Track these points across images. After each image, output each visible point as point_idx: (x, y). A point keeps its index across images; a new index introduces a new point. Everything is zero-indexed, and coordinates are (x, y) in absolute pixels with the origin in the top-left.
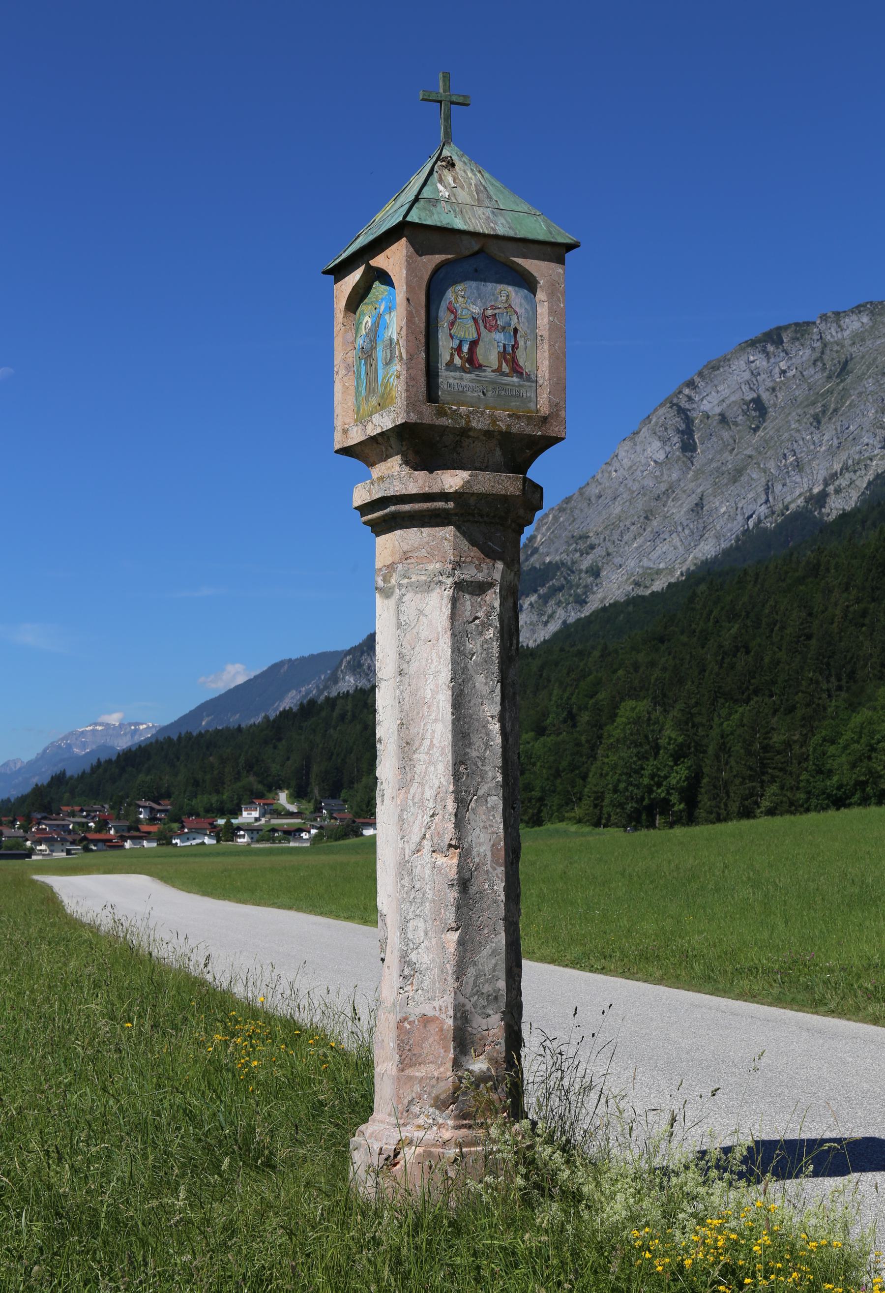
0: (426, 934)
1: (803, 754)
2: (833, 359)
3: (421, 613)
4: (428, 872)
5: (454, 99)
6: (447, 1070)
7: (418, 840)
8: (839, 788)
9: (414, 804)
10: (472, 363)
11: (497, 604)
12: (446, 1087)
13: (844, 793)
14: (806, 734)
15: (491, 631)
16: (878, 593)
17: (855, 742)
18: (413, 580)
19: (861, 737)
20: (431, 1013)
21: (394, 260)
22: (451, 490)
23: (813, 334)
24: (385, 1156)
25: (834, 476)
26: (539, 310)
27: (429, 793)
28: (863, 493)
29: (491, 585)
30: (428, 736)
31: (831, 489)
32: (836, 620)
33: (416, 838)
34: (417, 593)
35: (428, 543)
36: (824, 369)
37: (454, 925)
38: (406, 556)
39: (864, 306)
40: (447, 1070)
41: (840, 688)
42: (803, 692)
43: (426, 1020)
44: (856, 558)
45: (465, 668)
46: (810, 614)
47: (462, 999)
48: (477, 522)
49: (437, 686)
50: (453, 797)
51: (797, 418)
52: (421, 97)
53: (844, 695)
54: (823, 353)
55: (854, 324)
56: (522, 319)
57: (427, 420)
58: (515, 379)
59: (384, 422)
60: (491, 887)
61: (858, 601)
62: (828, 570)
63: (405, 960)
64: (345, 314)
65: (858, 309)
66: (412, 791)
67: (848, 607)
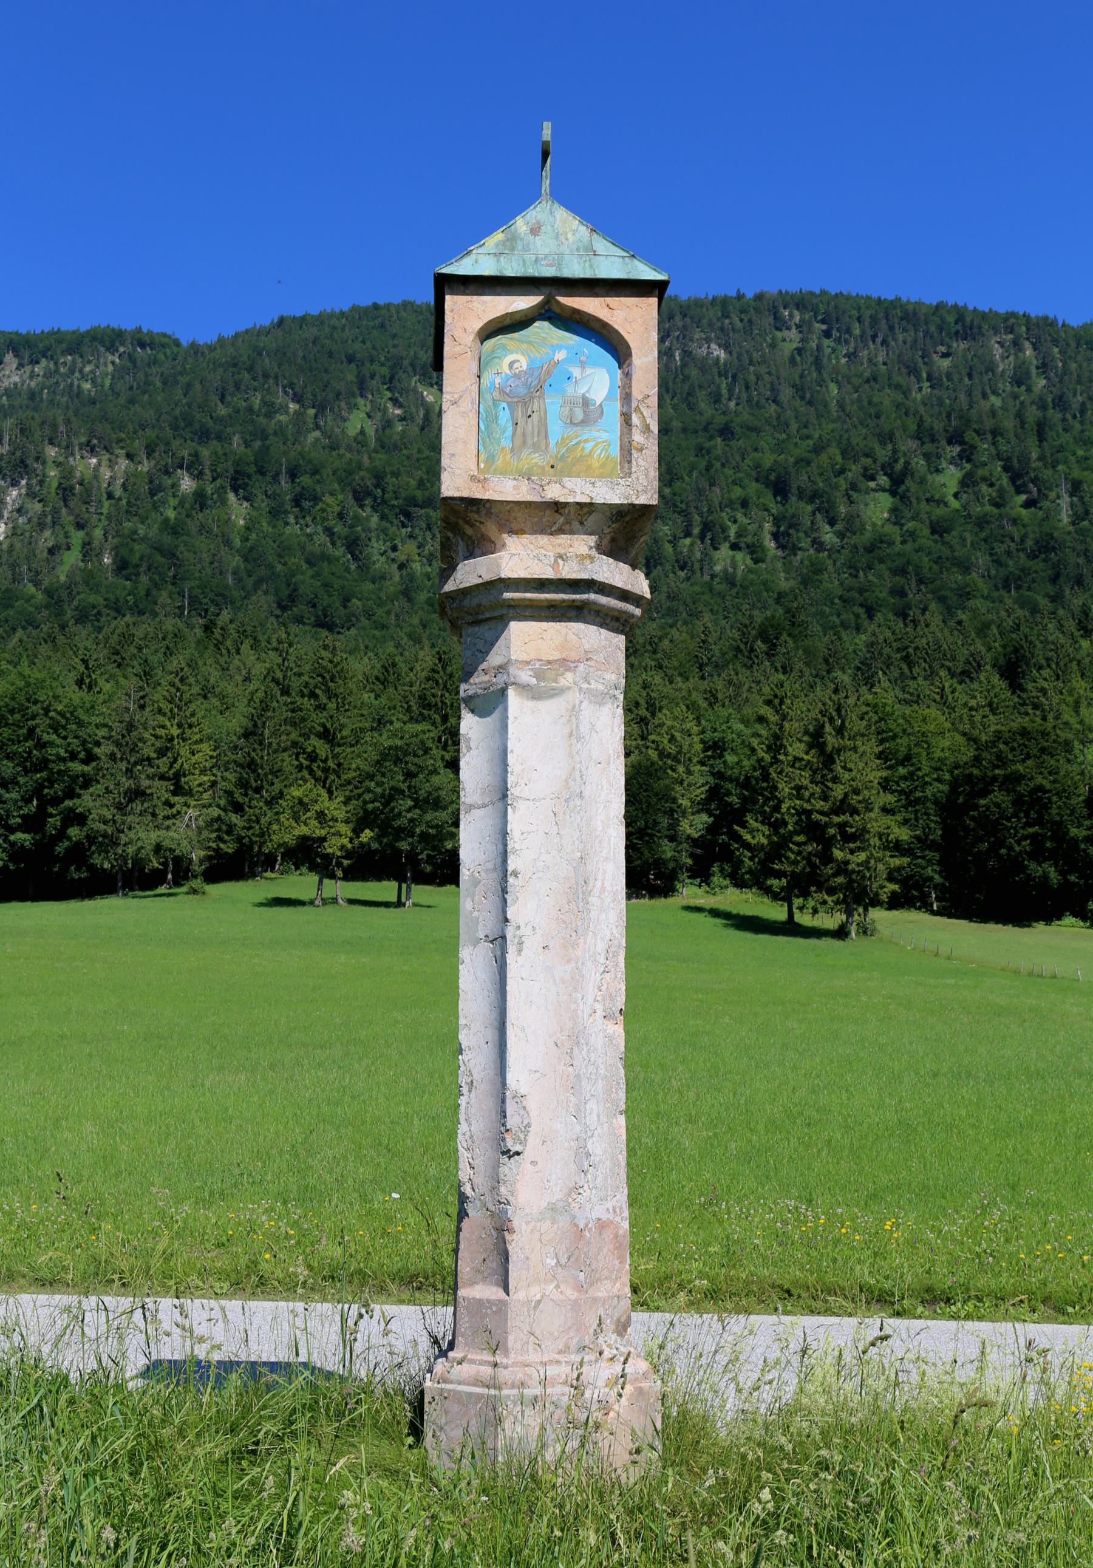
20: (605, 1217)
27: (601, 946)
30: (600, 877)
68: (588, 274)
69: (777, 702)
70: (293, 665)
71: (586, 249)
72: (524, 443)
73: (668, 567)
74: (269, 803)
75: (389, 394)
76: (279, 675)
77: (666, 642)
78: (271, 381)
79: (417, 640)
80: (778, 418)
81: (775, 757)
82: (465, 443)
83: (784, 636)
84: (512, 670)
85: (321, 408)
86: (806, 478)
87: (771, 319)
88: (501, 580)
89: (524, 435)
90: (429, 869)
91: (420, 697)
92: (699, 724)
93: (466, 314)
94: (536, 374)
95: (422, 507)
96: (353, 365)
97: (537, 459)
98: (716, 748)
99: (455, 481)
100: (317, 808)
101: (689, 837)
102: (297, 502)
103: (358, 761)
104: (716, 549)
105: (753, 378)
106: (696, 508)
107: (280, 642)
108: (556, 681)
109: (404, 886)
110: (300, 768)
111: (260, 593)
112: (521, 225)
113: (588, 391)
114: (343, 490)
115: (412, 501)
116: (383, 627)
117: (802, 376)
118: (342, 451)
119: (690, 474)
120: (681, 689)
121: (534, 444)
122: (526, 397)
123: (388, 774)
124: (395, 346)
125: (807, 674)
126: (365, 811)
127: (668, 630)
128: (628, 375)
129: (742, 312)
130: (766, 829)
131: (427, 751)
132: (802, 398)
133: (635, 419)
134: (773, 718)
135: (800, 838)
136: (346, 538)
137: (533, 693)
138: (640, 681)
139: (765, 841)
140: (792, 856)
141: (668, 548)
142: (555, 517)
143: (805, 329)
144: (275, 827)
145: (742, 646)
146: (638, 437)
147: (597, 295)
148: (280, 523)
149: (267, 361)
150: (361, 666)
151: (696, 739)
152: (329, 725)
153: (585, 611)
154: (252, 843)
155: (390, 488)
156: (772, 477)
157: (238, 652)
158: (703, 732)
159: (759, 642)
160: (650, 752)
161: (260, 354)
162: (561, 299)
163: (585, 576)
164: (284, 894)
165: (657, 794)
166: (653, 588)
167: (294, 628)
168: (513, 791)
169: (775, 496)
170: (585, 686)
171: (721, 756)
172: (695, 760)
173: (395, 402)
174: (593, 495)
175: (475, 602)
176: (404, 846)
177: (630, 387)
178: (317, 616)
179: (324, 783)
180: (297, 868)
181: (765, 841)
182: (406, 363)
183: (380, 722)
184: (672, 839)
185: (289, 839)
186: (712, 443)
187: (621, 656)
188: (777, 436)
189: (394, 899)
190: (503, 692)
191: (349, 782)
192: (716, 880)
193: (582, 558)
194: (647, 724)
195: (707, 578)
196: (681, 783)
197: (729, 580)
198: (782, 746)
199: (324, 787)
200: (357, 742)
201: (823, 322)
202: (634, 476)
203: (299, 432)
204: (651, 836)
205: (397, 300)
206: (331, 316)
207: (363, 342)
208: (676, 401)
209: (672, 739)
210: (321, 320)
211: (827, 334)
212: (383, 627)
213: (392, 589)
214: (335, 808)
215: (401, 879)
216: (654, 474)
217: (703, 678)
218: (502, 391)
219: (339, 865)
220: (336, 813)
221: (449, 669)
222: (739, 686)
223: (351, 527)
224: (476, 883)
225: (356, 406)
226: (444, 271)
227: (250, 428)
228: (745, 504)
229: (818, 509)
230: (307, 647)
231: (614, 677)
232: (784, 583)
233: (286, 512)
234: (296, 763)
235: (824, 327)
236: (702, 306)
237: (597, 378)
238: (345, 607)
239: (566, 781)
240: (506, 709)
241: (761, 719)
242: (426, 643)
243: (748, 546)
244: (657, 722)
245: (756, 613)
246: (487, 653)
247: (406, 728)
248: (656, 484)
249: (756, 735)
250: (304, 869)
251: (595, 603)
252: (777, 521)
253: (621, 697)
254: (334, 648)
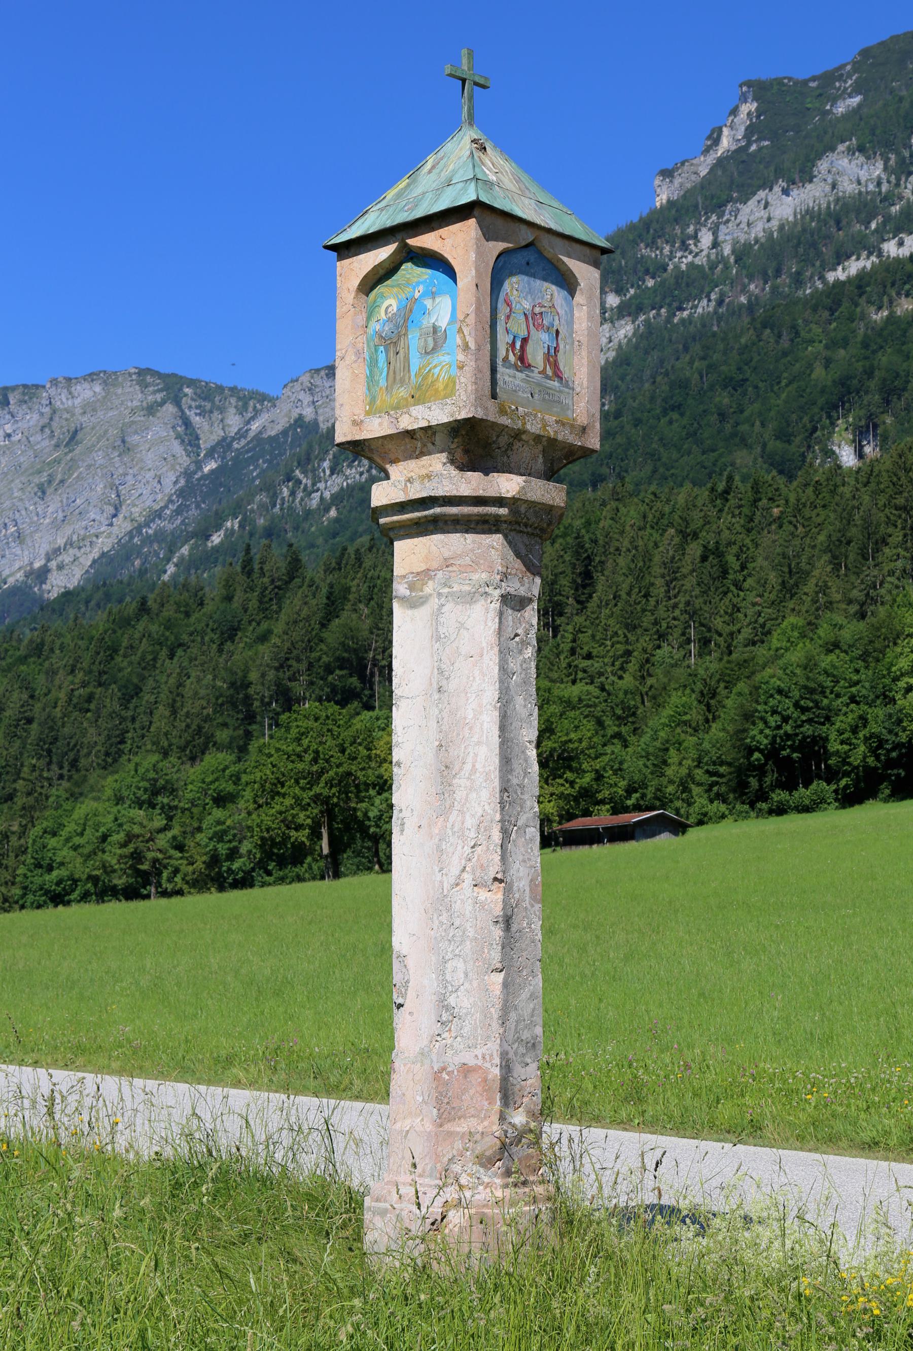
0: (466, 975)
1: (21, 846)
2: (62, 427)
3: (461, 626)
4: (469, 908)
5: (477, 79)
6: (492, 1123)
7: (458, 873)
8: (58, 883)
9: (453, 833)
10: (523, 362)
11: (535, 621)
12: (490, 1144)
13: (64, 889)
14: (26, 825)
15: (530, 650)
16: (105, 677)
17: (78, 835)
19: (84, 830)
20: (472, 1062)
21: (459, 243)
22: (509, 495)
23: (42, 398)
24: (431, 1220)
25: (57, 551)
26: (576, 314)
27: (470, 822)
28: (87, 571)
29: (530, 600)
30: (469, 760)
31: (53, 564)
32: (59, 704)
33: (455, 871)
34: (457, 603)
35: (472, 550)
36: (52, 436)
37: (499, 966)
38: (447, 564)
39: (98, 374)
40: (492, 1123)
41: (61, 777)
42: (24, 779)
43: (466, 1070)
44: (82, 639)
45: (508, 688)
46: (32, 697)
47: (507, 1047)
48: (521, 532)
49: (480, 706)
50: (499, 827)
51: (20, 486)
52: (448, 71)
53: (65, 784)
54: (51, 419)
55: (86, 392)
56: (562, 321)
57: (491, 418)
58: (556, 384)
59: (438, 414)
60: (529, 924)
61: (84, 685)
62: (52, 650)
63: (443, 1004)
64: (357, 295)
65: (91, 377)
66: (451, 819)
67: (72, 690)
142: (416, 442)
147: (433, 230)
153: (441, 524)
163: (424, 494)
174: (430, 418)
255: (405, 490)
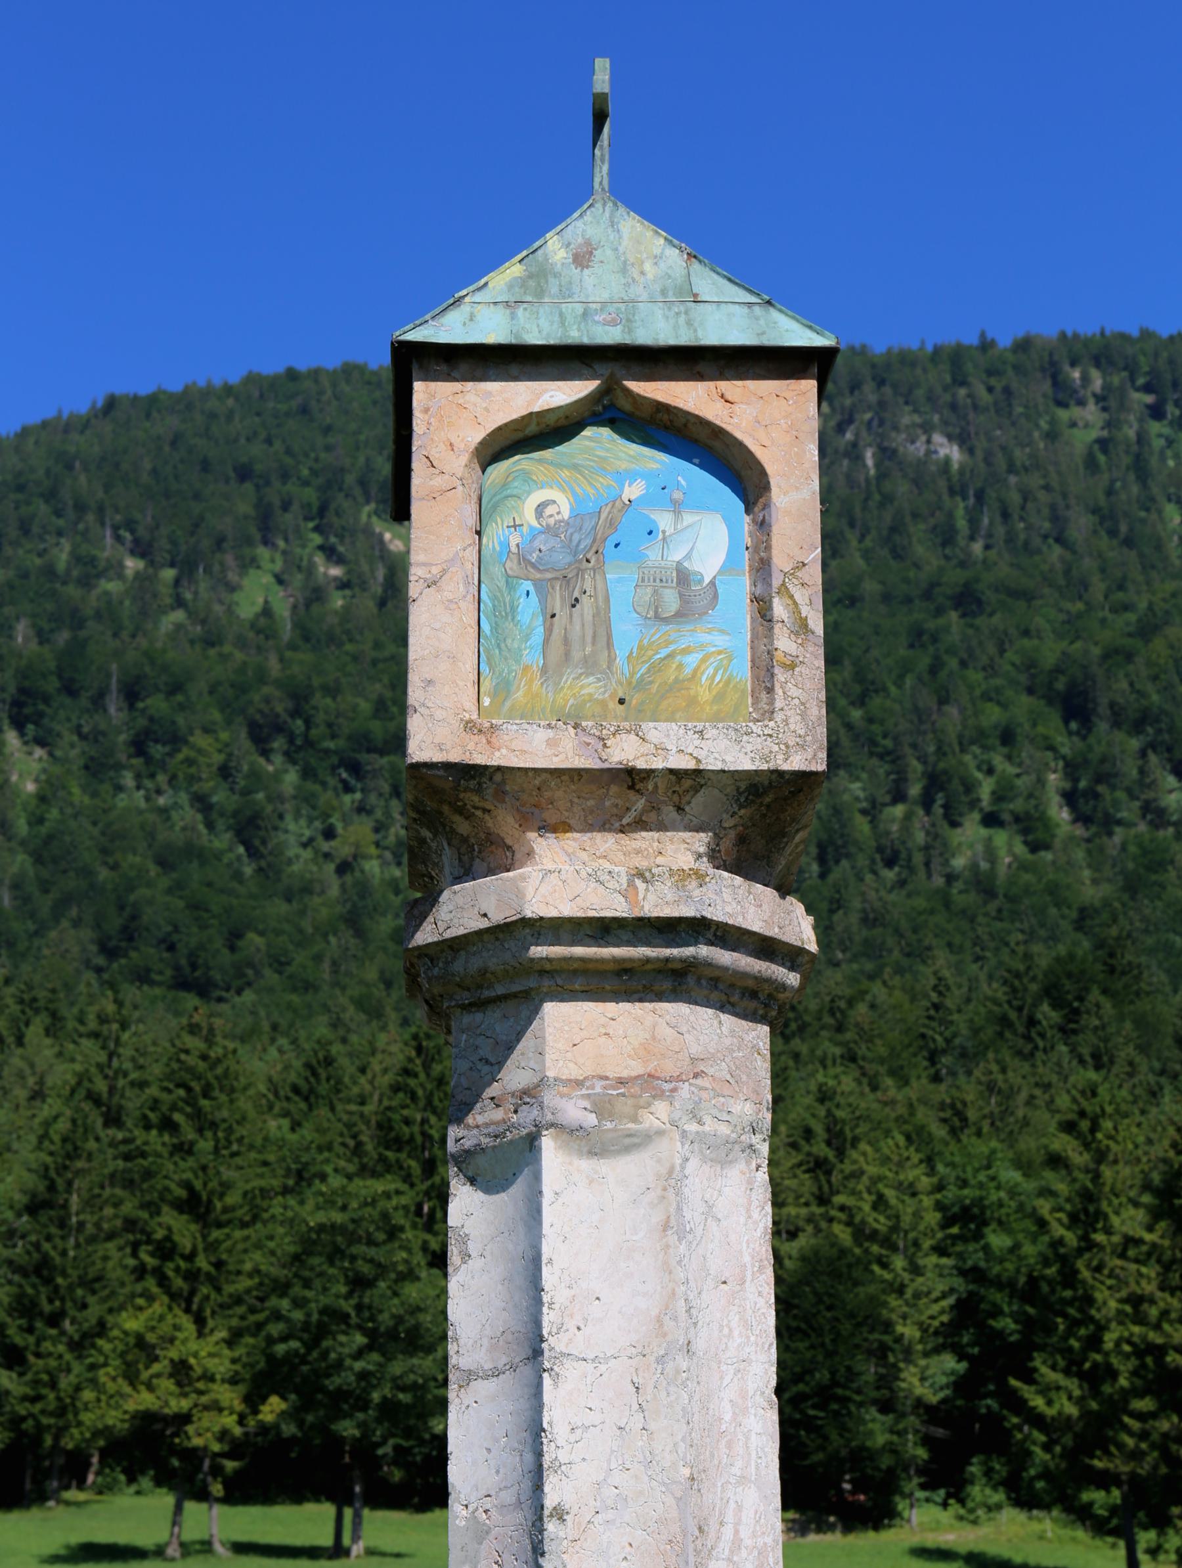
18: (707, 1128)
30: (729, 1518)
59: (732, 752)
68: (683, 338)
69: (1085, 1125)
70: (127, 1065)
71: (679, 291)
72: (567, 655)
73: (862, 861)
74: (78, 1346)
75: (317, 539)
76: (101, 1086)
77: (862, 1008)
78: (90, 517)
79: (375, 1013)
80: (1067, 572)
81: (1085, 1238)
82: (453, 658)
83: (1095, 995)
84: (549, 1098)
85: (187, 567)
86: (1124, 685)
87: (1047, 386)
88: (524, 922)
89: (566, 641)
90: (397, 1475)
91: (380, 1126)
92: (932, 1171)
93: (452, 419)
94: (588, 525)
95: (382, 753)
96: (248, 486)
97: (591, 687)
98: (967, 1220)
99: (432, 738)
100: (174, 1354)
101: (919, 1403)
102: (139, 746)
103: (257, 1256)
104: (954, 824)
105: (1015, 498)
106: (914, 746)
107: (103, 1019)
108: (635, 1119)
109: (348, 1513)
110: (140, 1272)
111: (65, 923)
112: (555, 248)
113: (688, 556)
114: (229, 722)
115: (364, 742)
116: (308, 986)
117: (1110, 492)
118: (227, 648)
119: (899, 682)
120: (893, 1103)
121: (585, 660)
122: (570, 568)
123: (318, 1283)
124: (328, 448)
125: (1144, 1068)
126: (271, 1358)
127: (865, 984)
128: (763, 526)
129: (990, 373)
130: (1073, 1385)
131: (393, 1233)
132: (1113, 533)
133: (779, 609)
134: (1079, 1158)
135: (1144, 1404)
136: (235, 814)
137: (587, 1143)
138: (813, 1087)
139: (1072, 1410)
140: (1130, 1442)
141: (862, 825)
142: (629, 798)
143: (1113, 403)
144: (88, 1395)
145: (1013, 1015)
146: (784, 643)
147: (701, 377)
148: (106, 787)
149: (83, 479)
150: (263, 1065)
151: (927, 1201)
152: (198, 1185)
153: (691, 980)
154: (40, 1429)
155: (320, 717)
156: (1060, 685)
157: (20, 1041)
158: (940, 1188)
159: (1045, 1007)
160: (837, 1228)
161: (70, 467)
162: (634, 386)
163: (688, 911)
164: (102, 1537)
165: (852, 1315)
166: (823, 930)
167: (131, 993)
168: (554, 1343)
169: (1066, 722)
170: (693, 1127)
171: (978, 1236)
172: (927, 1244)
173: (330, 553)
174: (701, 755)
175: (475, 964)
176: (348, 1429)
177: (768, 548)
178: (177, 968)
179: (189, 1301)
180: (131, 1480)
181: (1072, 1410)
182: (350, 479)
183: (302, 1177)
184: (886, 1407)
185: (115, 1419)
186: (941, 621)
187: (762, 1068)
188: (1068, 606)
189: (327, 1541)
190: (531, 1142)
191: (238, 1300)
192: (978, 1491)
193: (681, 876)
194: (828, 1173)
195: (939, 881)
196: (900, 1290)
197: (984, 885)
198: (1100, 1215)
199: (187, 1310)
200: (255, 1218)
201: (1147, 389)
202: (779, 717)
203: (144, 613)
204: (844, 1400)
205: (332, 362)
206: (207, 393)
207: (269, 441)
208: (868, 542)
209: (880, 1203)
210: (187, 401)
211: (1156, 412)
212: (308, 986)
213: (324, 912)
214: (210, 1352)
215: (341, 1498)
216: (818, 711)
217: (936, 1079)
218: (522, 559)
219: (217, 1471)
220: (212, 1364)
221: (437, 1069)
222: (1008, 1095)
223: (246, 792)
224: (481, 1533)
225: (254, 562)
226: (411, 336)
227: (50, 606)
228: (1007, 737)
229: (1153, 746)
230: (157, 1029)
231: (749, 1108)
232: (1089, 889)
233: (118, 767)
234: (131, 1262)
235: (1149, 399)
236: (913, 364)
237: (704, 533)
238: (232, 949)
239: (659, 1321)
240: (537, 1177)
241: (1056, 1161)
242: (393, 1017)
243: (1017, 819)
244: (848, 1167)
245: (1037, 948)
246: (500, 1064)
247: (352, 1188)
248: (822, 732)
249: (1046, 1192)
250: (146, 1482)
251: (708, 964)
252: (1072, 769)
253: (765, 1149)
254: (211, 1030)
255: (629, 893)
